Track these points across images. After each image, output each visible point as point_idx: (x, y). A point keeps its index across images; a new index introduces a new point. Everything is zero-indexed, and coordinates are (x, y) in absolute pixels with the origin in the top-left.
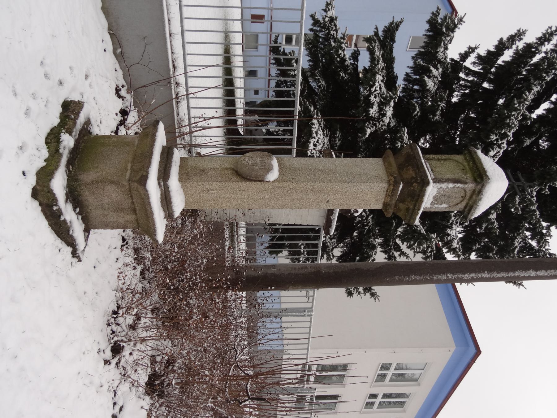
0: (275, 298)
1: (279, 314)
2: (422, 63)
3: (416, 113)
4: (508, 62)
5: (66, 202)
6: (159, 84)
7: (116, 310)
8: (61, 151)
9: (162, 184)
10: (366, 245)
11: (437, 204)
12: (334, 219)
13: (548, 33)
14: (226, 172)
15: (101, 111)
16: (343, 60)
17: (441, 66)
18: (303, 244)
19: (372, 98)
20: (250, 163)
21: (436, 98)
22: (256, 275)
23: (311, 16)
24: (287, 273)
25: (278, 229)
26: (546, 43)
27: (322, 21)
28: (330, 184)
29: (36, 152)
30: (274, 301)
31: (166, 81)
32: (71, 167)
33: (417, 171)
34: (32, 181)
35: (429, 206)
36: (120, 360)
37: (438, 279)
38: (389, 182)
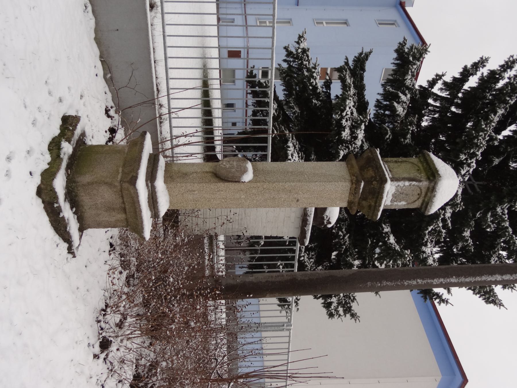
0: (254, 312)
1: (259, 327)
2: (391, 89)
3: (388, 136)
4: (474, 87)
5: (65, 201)
6: (145, 105)
7: (104, 308)
8: (62, 156)
9: (150, 185)
10: (343, 265)
11: (396, 201)
12: (308, 229)
13: (510, 61)
14: (206, 174)
15: (93, 128)
16: (315, 88)
17: (409, 92)
18: (282, 264)
19: (344, 121)
20: (228, 166)
21: (405, 123)
22: (235, 283)
23: (285, 48)
24: (264, 281)
25: (258, 250)
26: (509, 70)
27: (295, 53)
28: (299, 184)
29: (41, 156)
30: (253, 316)
31: (151, 102)
32: (69, 171)
33: (376, 171)
34: (37, 180)
35: (388, 203)
36: (107, 355)
37: (408, 285)
38: (352, 181)
